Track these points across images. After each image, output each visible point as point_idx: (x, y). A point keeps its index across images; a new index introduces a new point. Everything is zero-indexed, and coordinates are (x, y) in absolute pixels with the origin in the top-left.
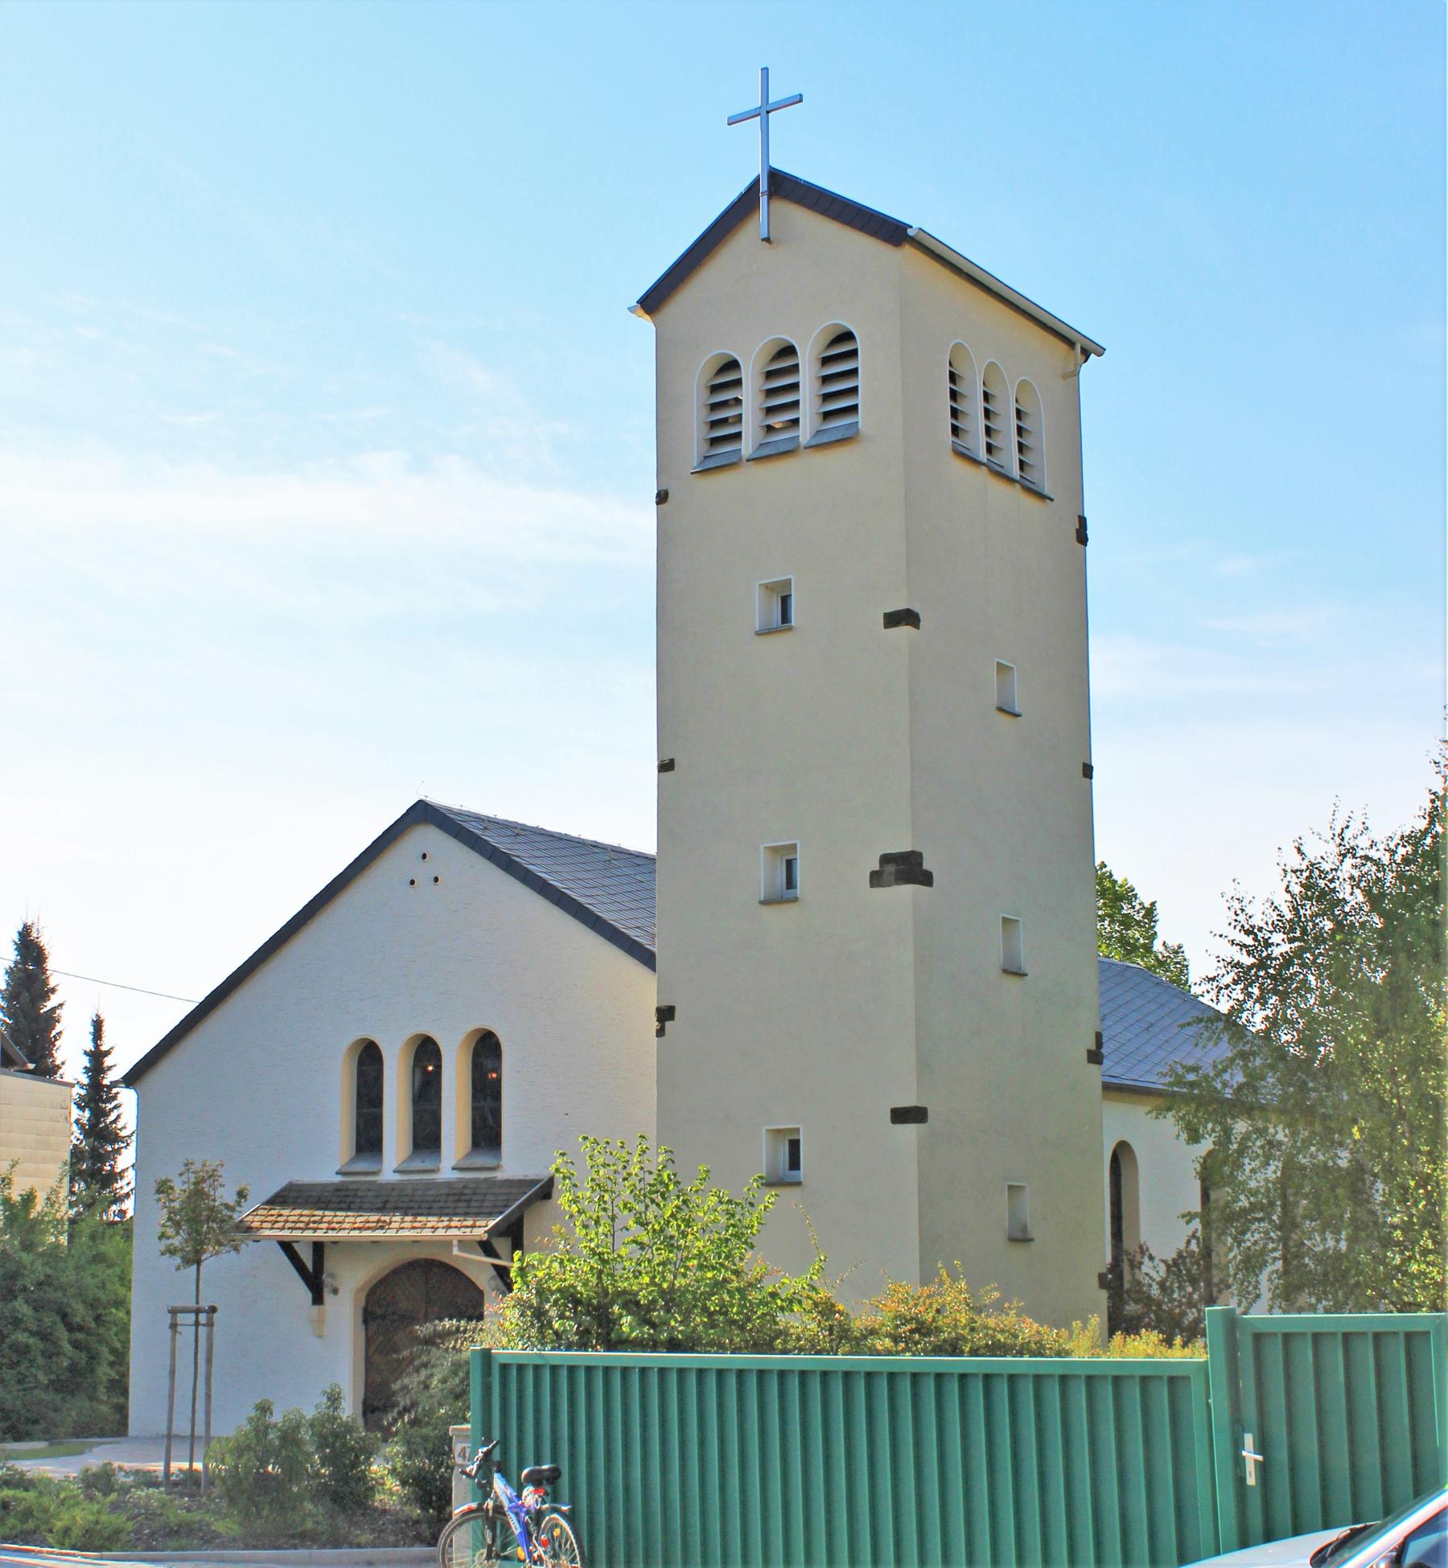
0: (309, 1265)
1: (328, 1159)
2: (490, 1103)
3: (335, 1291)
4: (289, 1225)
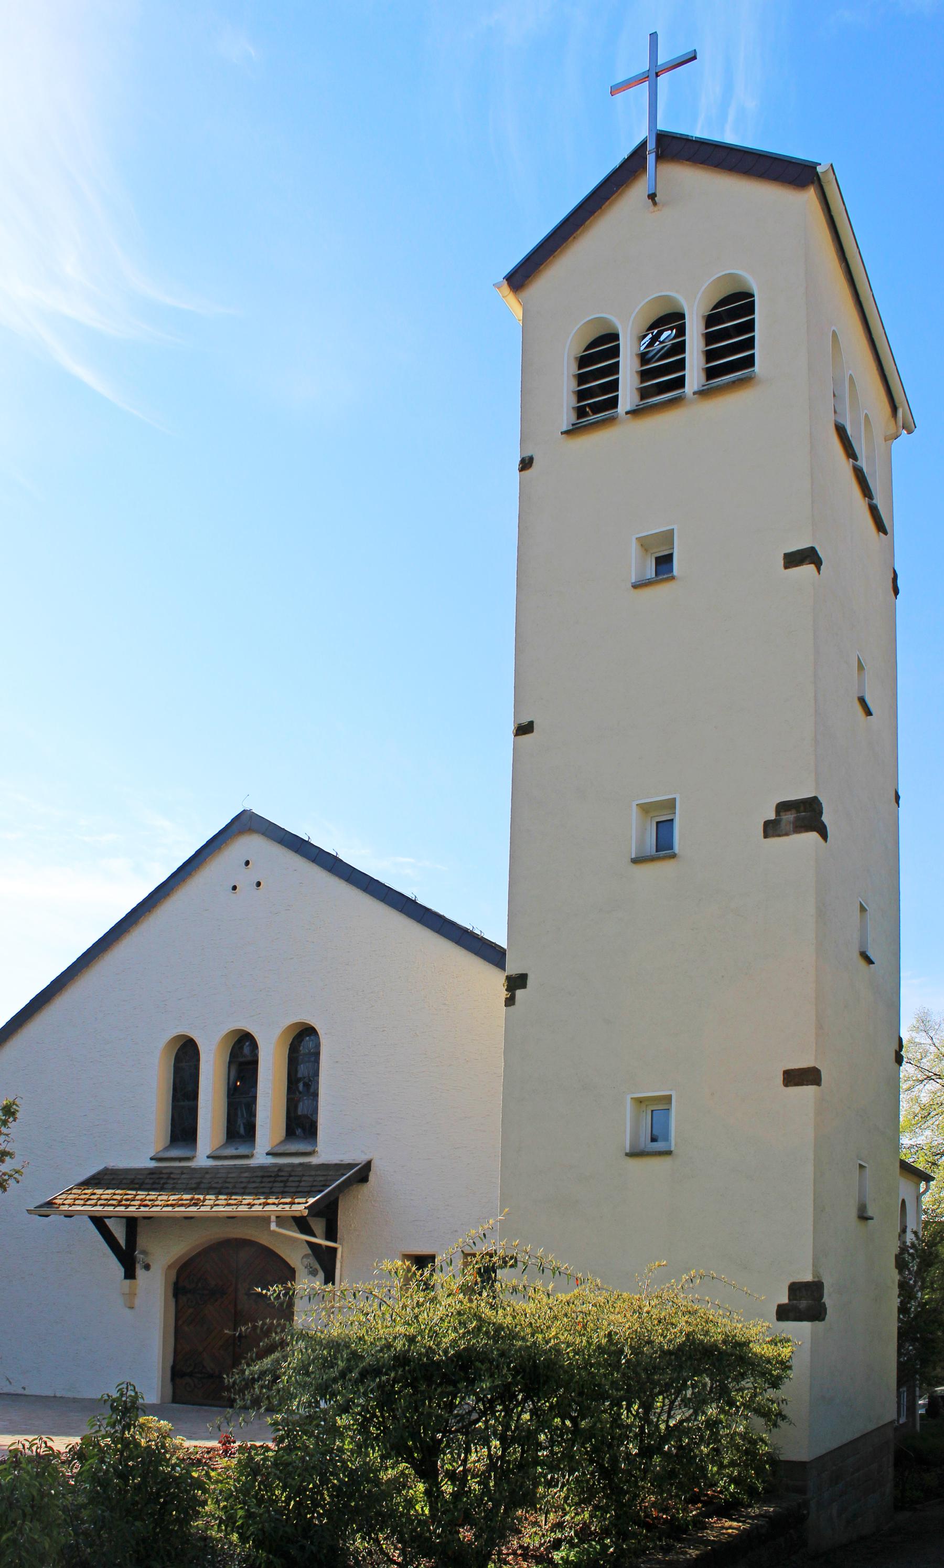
0: (122, 1243)
1: (144, 1144)
2: (302, 1109)
3: (147, 1267)
4: (100, 1202)
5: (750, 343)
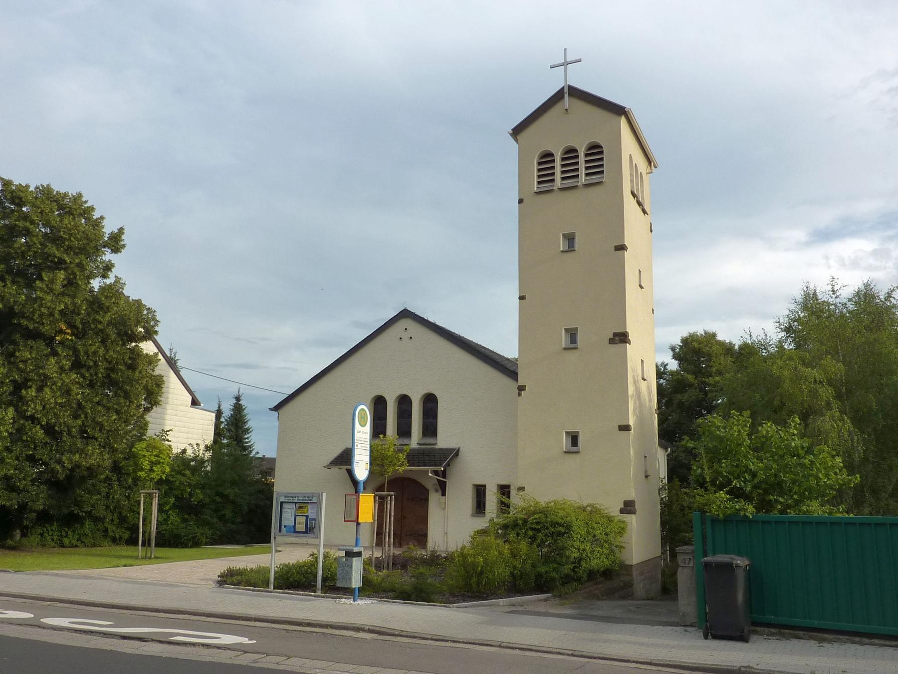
5: (602, 159)
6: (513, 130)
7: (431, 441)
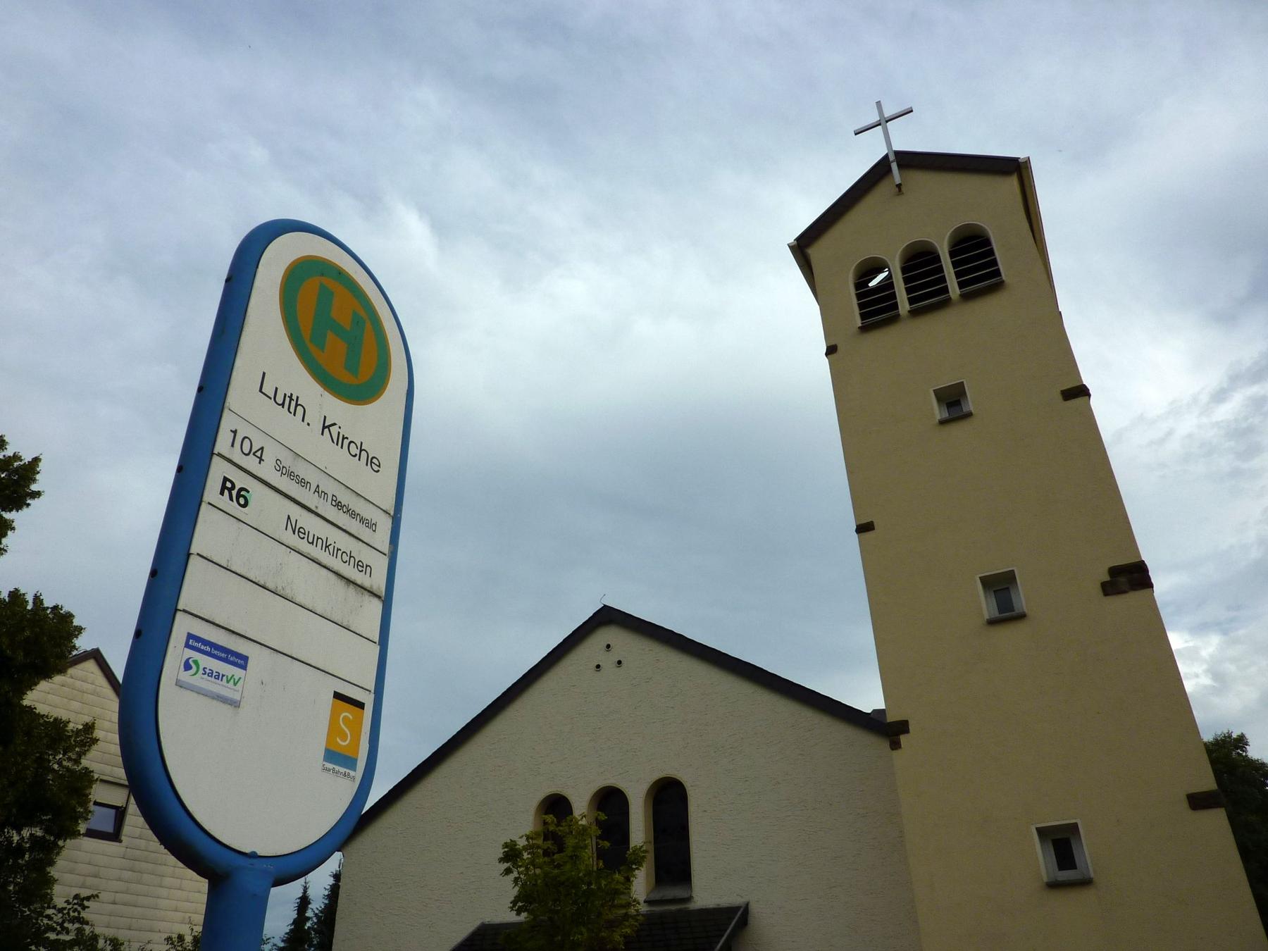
6: (798, 239)
7: (677, 892)
